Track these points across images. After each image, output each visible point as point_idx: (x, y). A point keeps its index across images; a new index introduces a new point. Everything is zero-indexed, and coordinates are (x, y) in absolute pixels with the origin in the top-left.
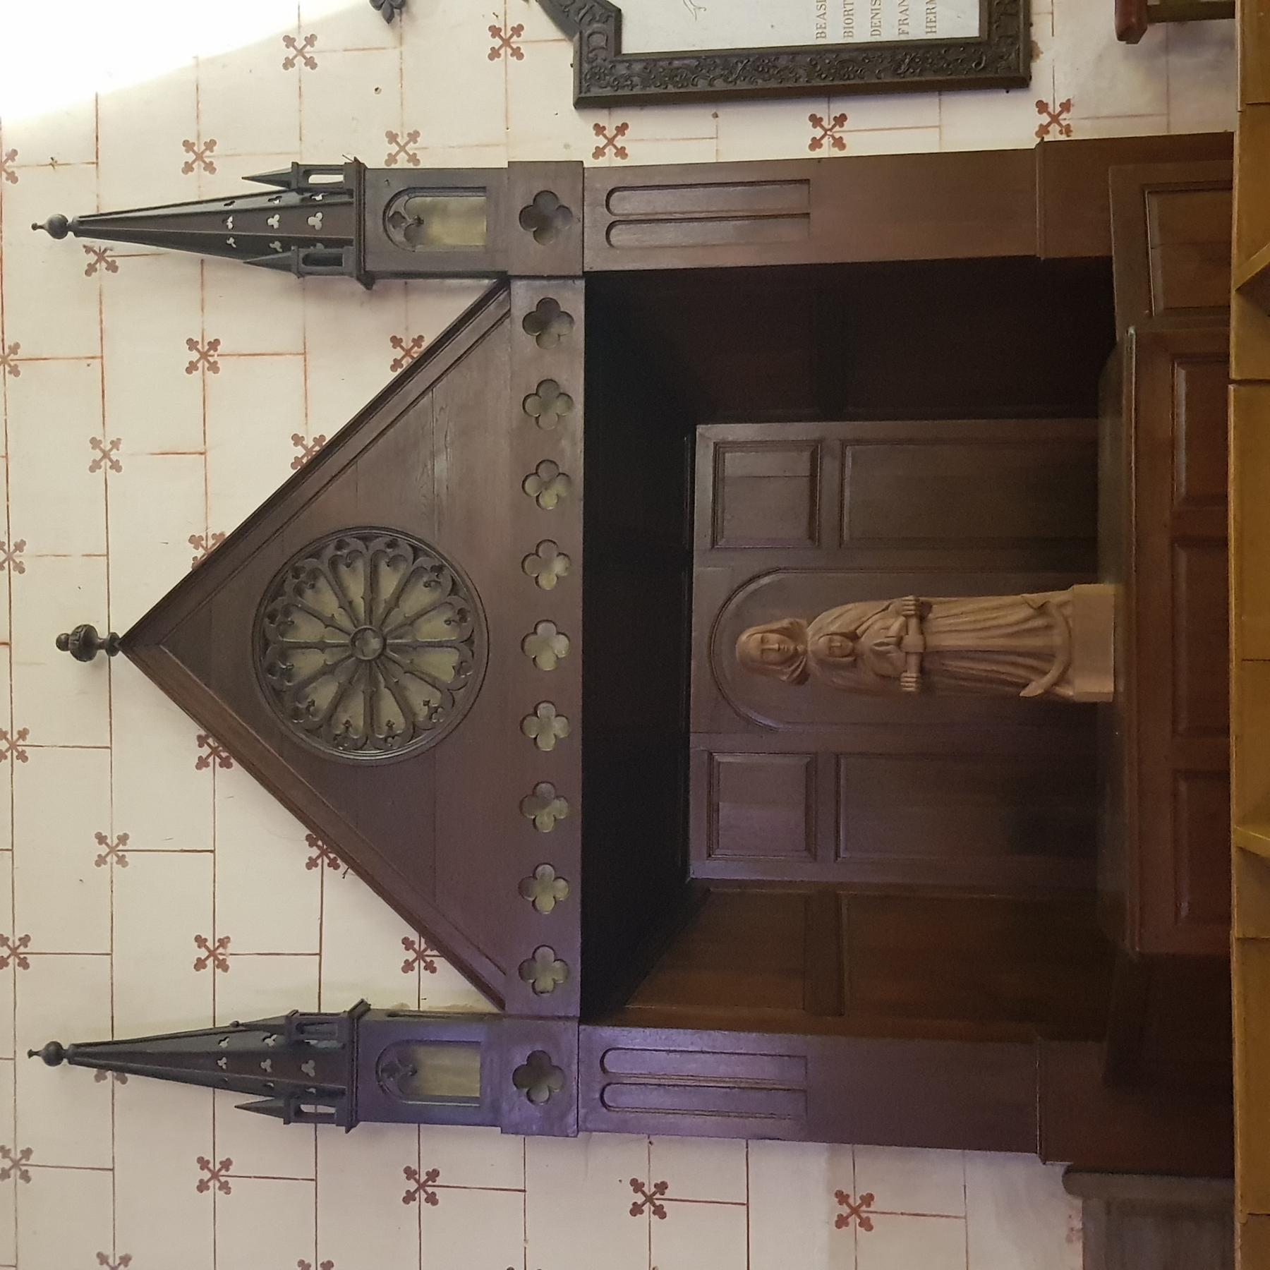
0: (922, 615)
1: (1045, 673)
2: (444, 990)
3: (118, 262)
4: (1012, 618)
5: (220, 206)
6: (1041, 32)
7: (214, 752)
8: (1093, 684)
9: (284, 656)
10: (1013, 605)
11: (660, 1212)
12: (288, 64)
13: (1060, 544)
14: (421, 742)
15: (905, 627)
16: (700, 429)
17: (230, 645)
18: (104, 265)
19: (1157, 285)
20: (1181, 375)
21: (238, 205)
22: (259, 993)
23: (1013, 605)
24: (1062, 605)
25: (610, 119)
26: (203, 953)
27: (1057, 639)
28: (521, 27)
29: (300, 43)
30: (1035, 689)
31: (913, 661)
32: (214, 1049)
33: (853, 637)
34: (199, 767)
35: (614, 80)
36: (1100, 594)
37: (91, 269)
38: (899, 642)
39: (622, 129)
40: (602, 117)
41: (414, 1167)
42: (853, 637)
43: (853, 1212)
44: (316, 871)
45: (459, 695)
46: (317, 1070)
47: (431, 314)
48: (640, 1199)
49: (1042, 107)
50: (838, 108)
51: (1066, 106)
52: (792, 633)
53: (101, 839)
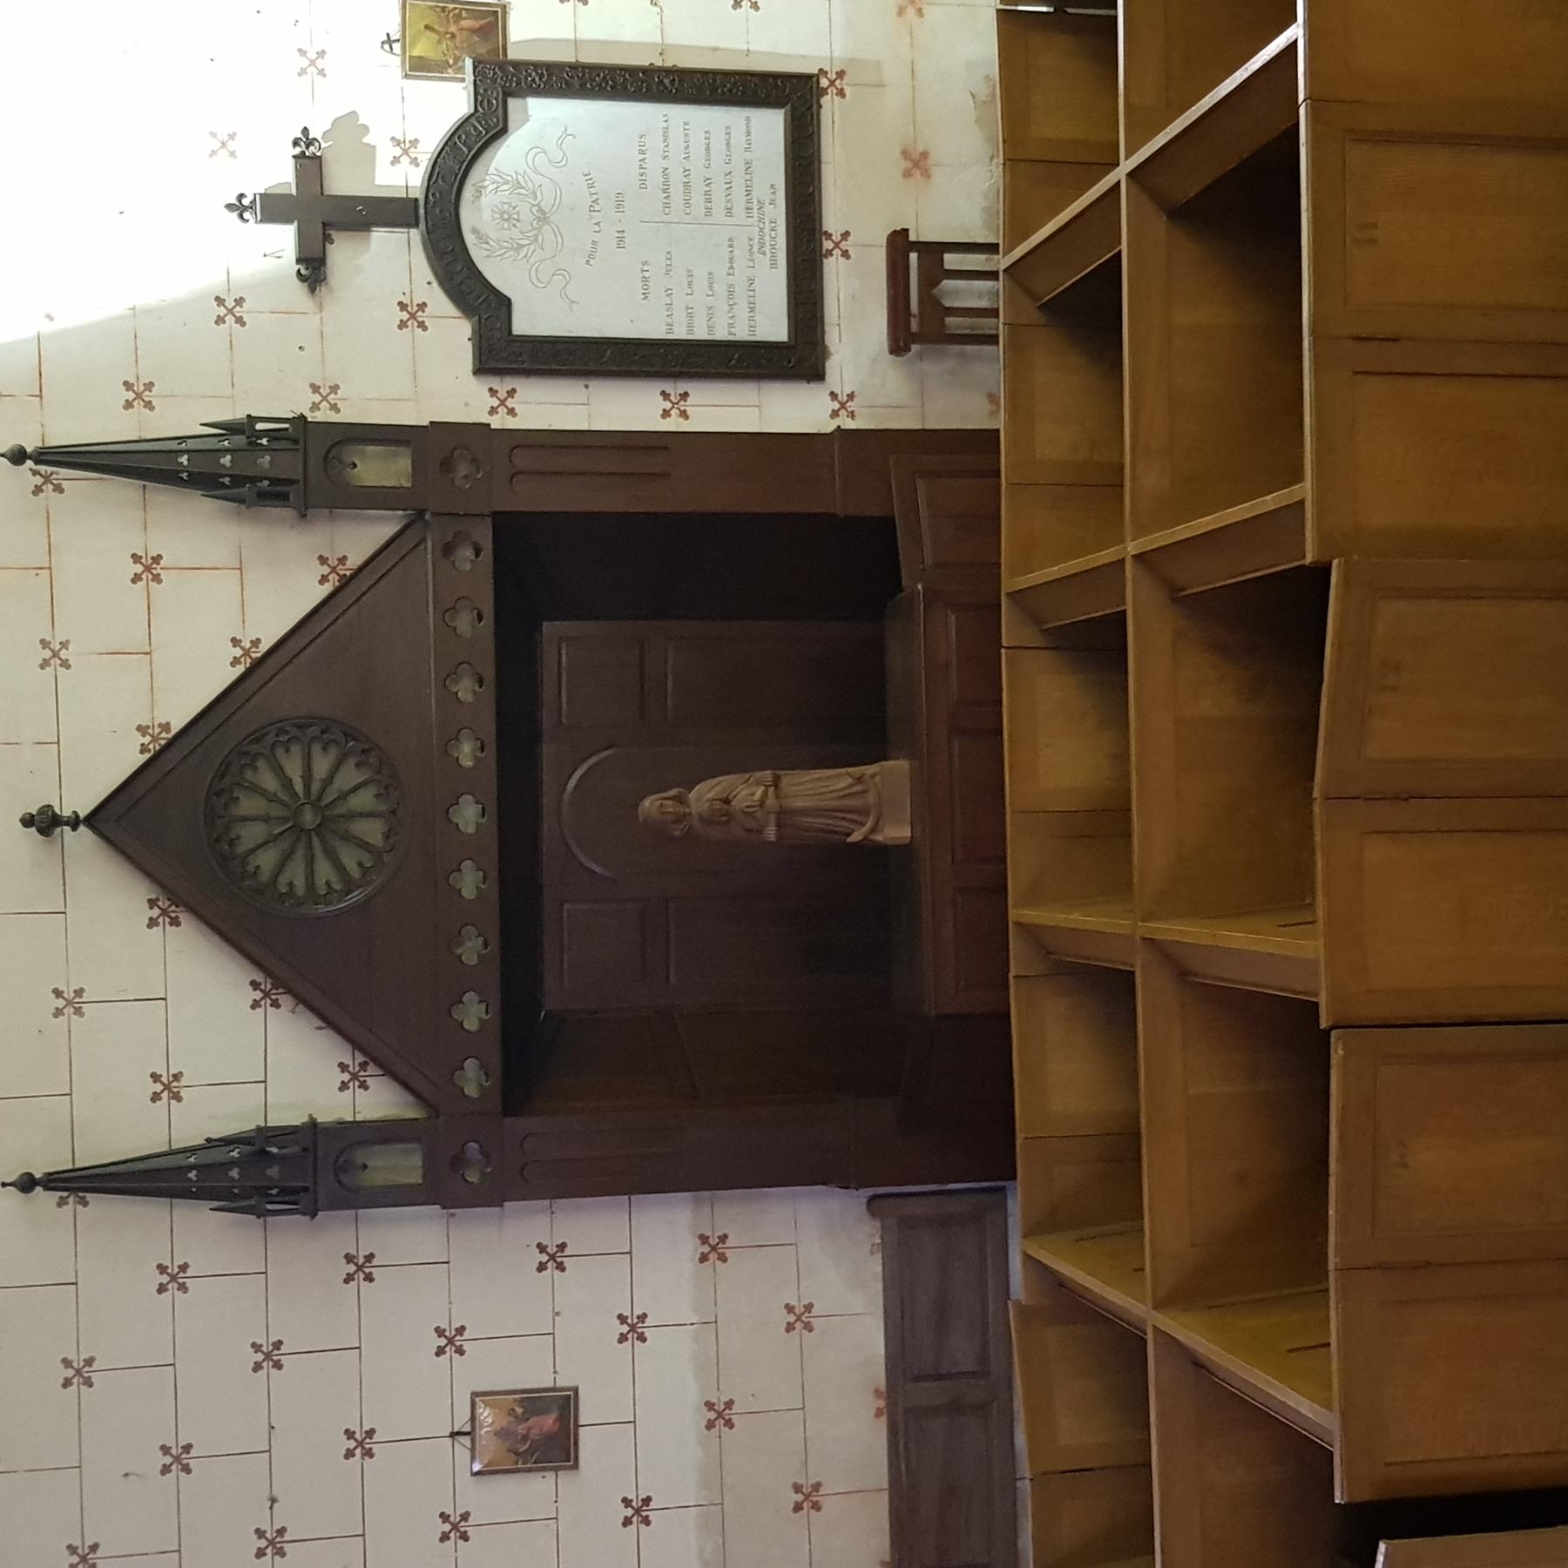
0: (776, 783)
1: (862, 825)
2: (379, 1101)
3: (65, 484)
4: (840, 786)
5: (173, 445)
6: (832, 338)
7: (164, 912)
8: (897, 832)
9: (228, 829)
10: (837, 776)
11: (561, 1267)
12: (220, 320)
13: (852, 723)
14: (356, 896)
15: (765, 793)
16: (546, 626)
17: (185, 822)
18: (51, 487)
19: (928, 550)
20: (952, 618)
21: (191, 444)
22: (210, 1115)
23: (837, 776)
24: (874, 776)
25: (503, 385)
26: (158, 1087)
27: (871, 798)
28: (424, 304)
29: (230, 304)
30: (856, 837)
31: (772, 818)
32: (183, 1163)
33: (727, 801)
34: (149, 926)
35: (504, 352)
36: (899, 767)
37: (38, 490)
38: (762, 804)
39: (511, 393)
40: (495, 383)
41: (353, 1252)
42: (727, 801)
43: (713, 1249)
44: (260, 1011)
45: (386, 858)
46: (272, 1176)
47: (359, 539)
48: (544, 1258)
49: (833, 395)
50: (682, 386)
51: (851, 396)
52: (679, 799)
53: (58, 993)
